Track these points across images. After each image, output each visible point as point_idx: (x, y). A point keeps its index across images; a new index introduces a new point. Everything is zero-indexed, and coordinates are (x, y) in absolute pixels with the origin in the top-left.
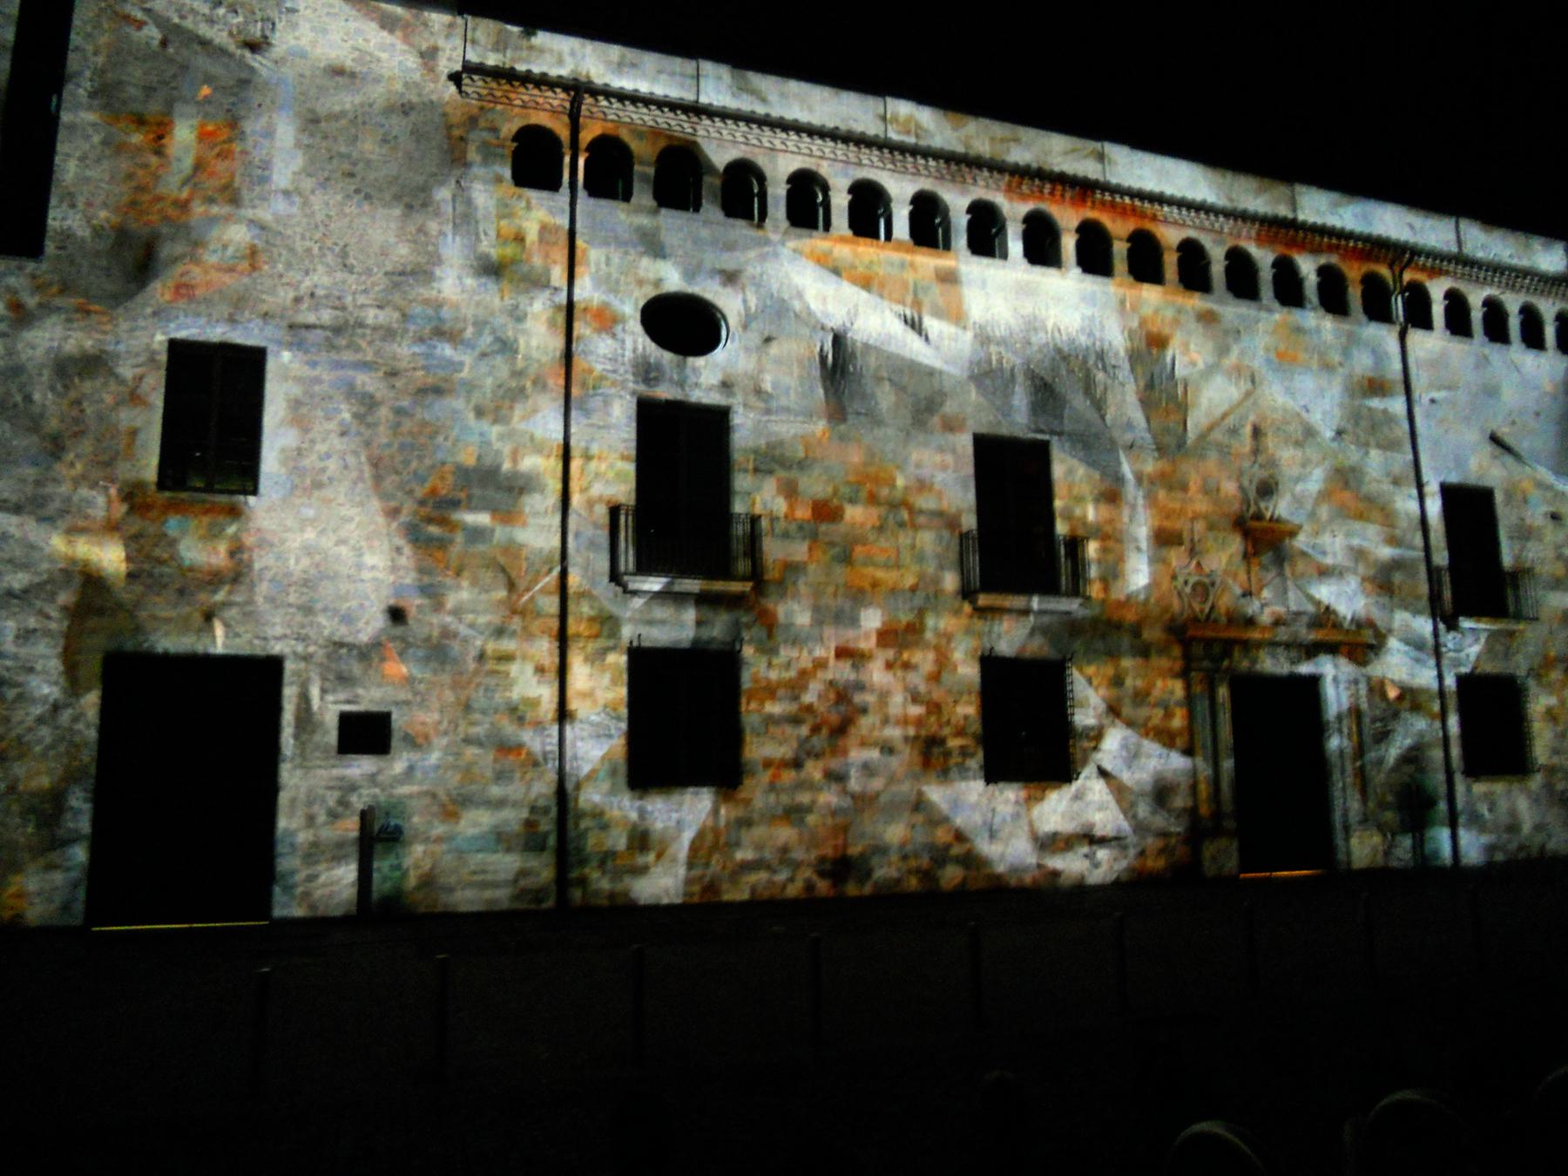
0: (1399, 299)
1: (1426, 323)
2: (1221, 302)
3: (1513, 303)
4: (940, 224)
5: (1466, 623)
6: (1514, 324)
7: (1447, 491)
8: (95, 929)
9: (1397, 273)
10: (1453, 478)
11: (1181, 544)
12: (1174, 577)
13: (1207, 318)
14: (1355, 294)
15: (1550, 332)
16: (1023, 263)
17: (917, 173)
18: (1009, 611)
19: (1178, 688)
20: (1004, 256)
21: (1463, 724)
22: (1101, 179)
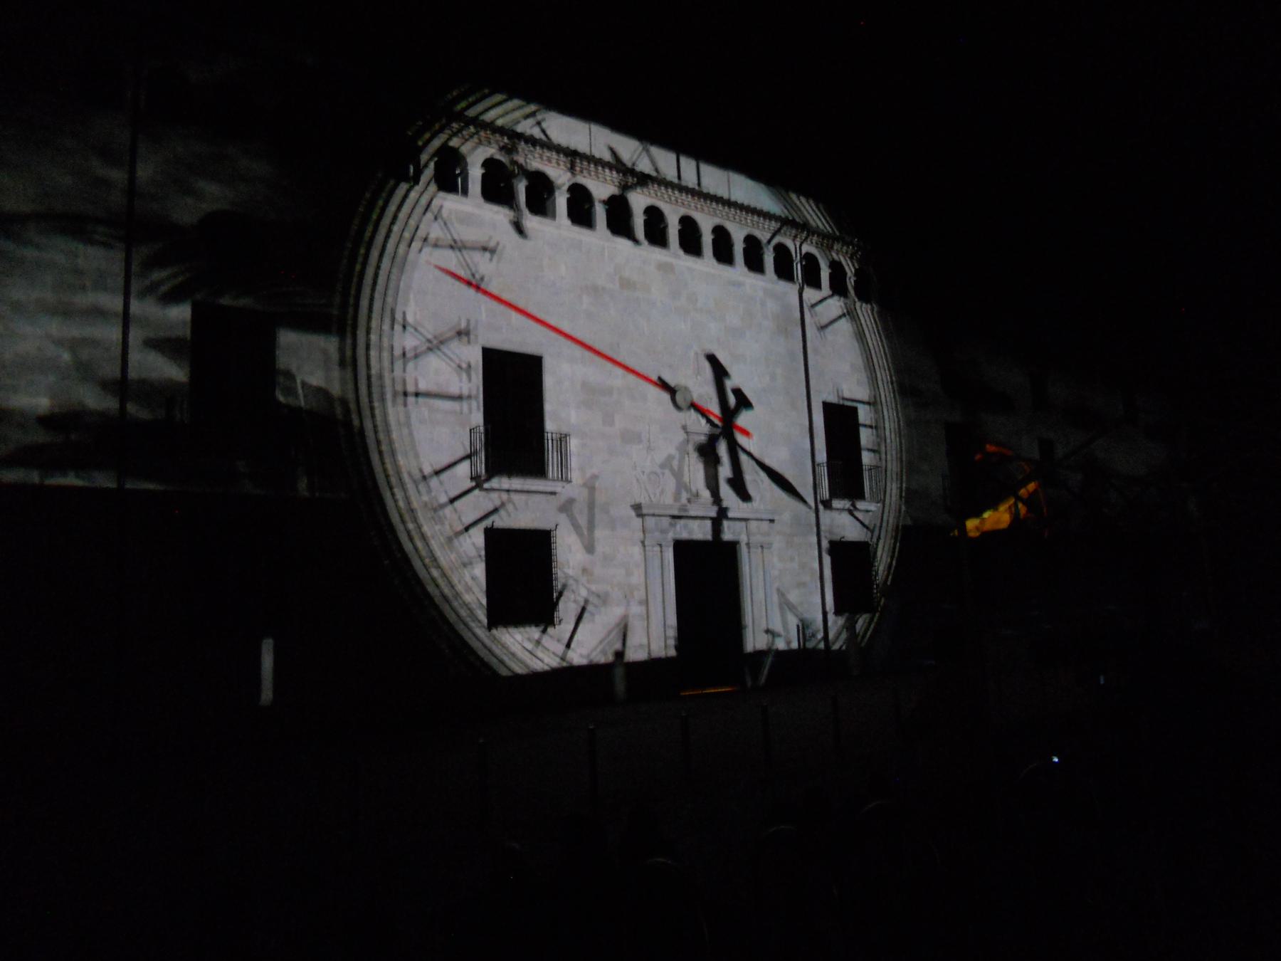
0: (799, 265)
1: (817, 285)
2: (677, 256)
3: (706, 223)
4: (459, 175)
5: (837, 503)
6: (707, 239)
7: (827, 407)
8: (267, 695)
9: (798, 246)
10: (832, 399)
11: (640, 441)
12: (635, 467)
13: (665, 268)
14: (769, 259)
15: (851, 281)
16: (567, 222)
17: (715, 215)
18: (901, 484)
19: (637, 550)
20: (553, 216)
21: (896, 563)
22: (588, 153)
